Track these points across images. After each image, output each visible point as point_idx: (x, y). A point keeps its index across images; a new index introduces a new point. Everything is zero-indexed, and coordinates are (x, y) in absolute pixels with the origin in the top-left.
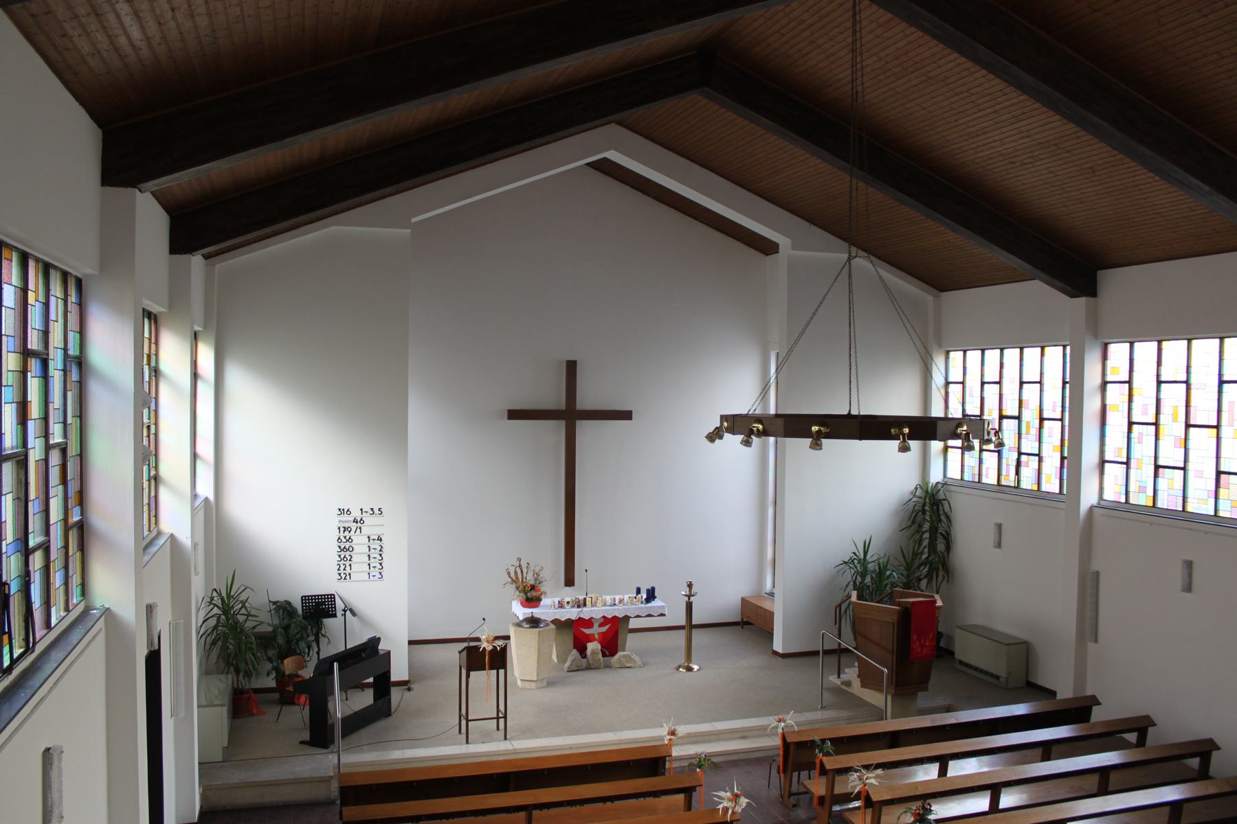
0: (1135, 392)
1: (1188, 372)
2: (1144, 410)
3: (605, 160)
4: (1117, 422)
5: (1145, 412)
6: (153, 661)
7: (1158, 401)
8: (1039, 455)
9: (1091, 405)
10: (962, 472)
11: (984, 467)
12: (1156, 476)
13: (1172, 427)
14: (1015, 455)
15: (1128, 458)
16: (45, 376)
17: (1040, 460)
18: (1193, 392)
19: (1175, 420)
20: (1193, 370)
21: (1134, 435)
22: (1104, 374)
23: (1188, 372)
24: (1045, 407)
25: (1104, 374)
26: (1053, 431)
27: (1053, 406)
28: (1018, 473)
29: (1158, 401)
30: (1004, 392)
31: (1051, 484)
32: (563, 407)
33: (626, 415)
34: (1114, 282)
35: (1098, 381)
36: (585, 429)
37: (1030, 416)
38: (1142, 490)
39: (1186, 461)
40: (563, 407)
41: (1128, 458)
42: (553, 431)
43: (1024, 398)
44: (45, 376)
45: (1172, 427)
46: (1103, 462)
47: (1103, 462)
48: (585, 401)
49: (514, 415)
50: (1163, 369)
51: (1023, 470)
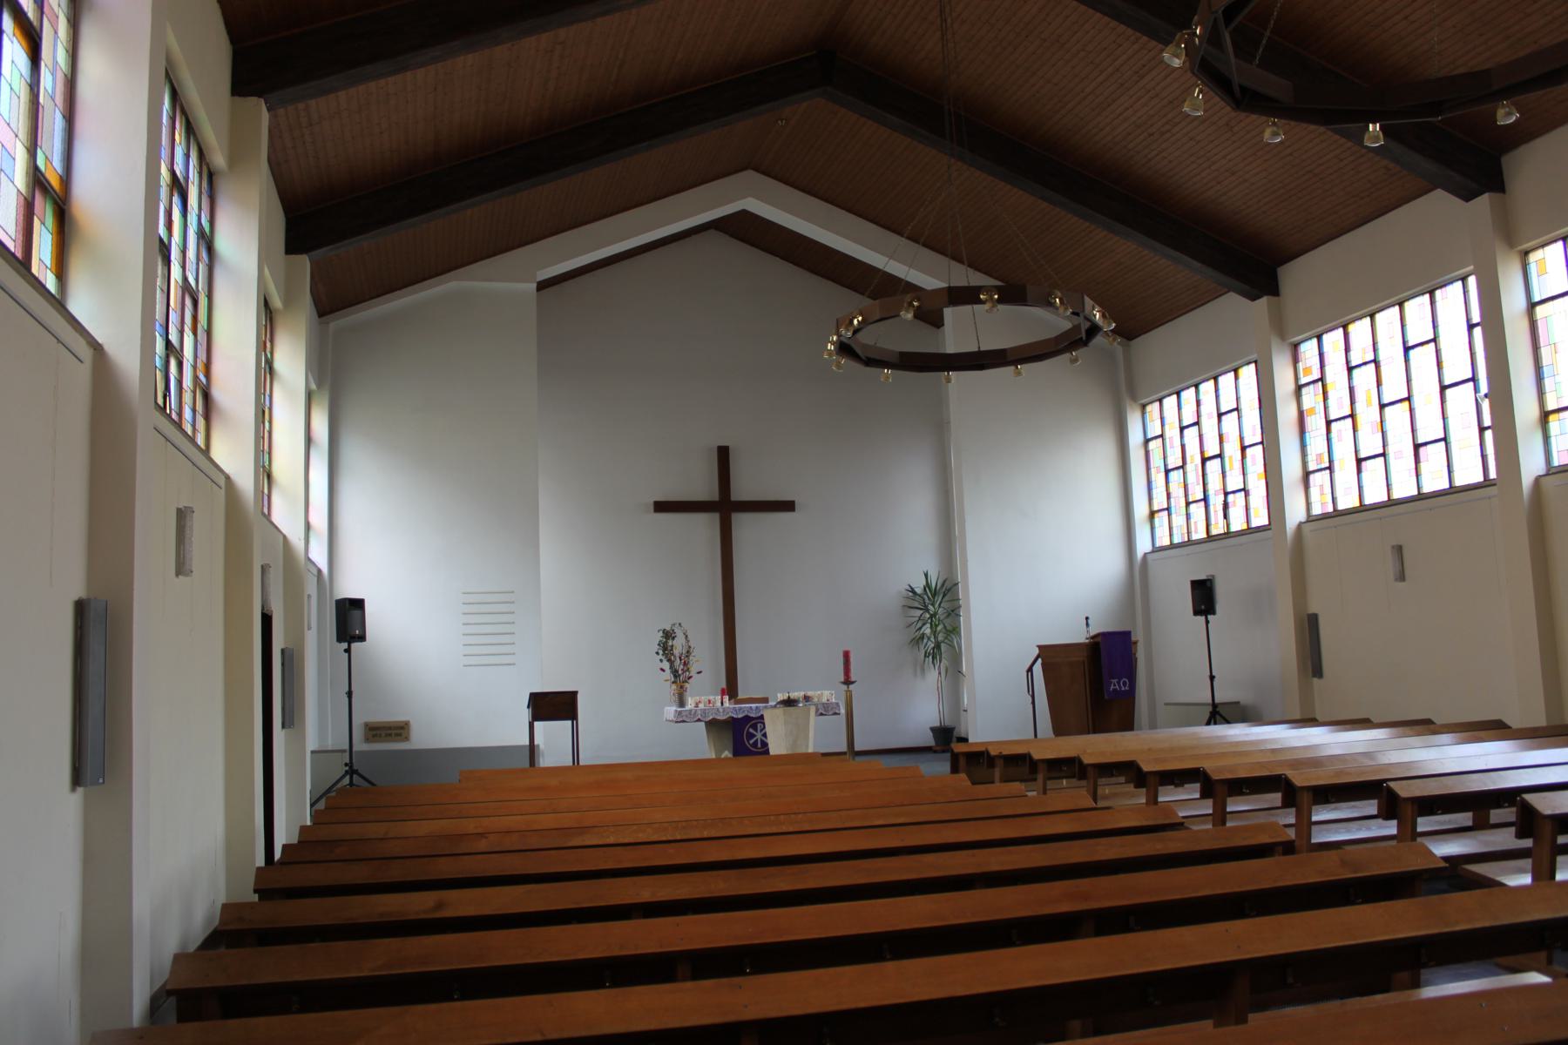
0: (1329, 388)
1: (1375, 350)
2: (1339, 407)
3: (744, 215)
4: (1316, 424)
5: (1341, 407)
6: (267, 620)
7: (1351, 390)
8: (1245, 490)
9: (1286, 414)
10: (1171, 535)
11: (1192, 521)
12: (1359, 471)
13: (1367, 414)
14: (1222, 497)
15: (1331, 461)
16: (180, 365)
17: (1247, 494)
18: (1383, 369)
19: (1369, 404)
20: (1380, 346)
21: (1334, 435)
22: (1297, 378)
23: (1375, 350)
24: (1245, 434)
25: (1297, 378)
26: (1256, 454)
27: (1253, 434)
28: (1225, 516)
29: (1351, 390)
30: (1204, 431)
31: (1260, 518)
32: (716, 498)
33: (788, 506)
34: (1294, 276)
35: (1291, 386)
36: (744, 524)
37: (1232, 450)
38: (1319, 456)
39: (1384, 446)
40: (716, 498)
41: (1331, 461)
42: (704, 527)
43: (1224, 431)
44: (180, 365)
45: (1367, 414)
46: (1307, 475)
47: (1307, 475)
48: (742, 490)
49: (661, 507)
50: (1384, 387)
51: (1232, 511)
